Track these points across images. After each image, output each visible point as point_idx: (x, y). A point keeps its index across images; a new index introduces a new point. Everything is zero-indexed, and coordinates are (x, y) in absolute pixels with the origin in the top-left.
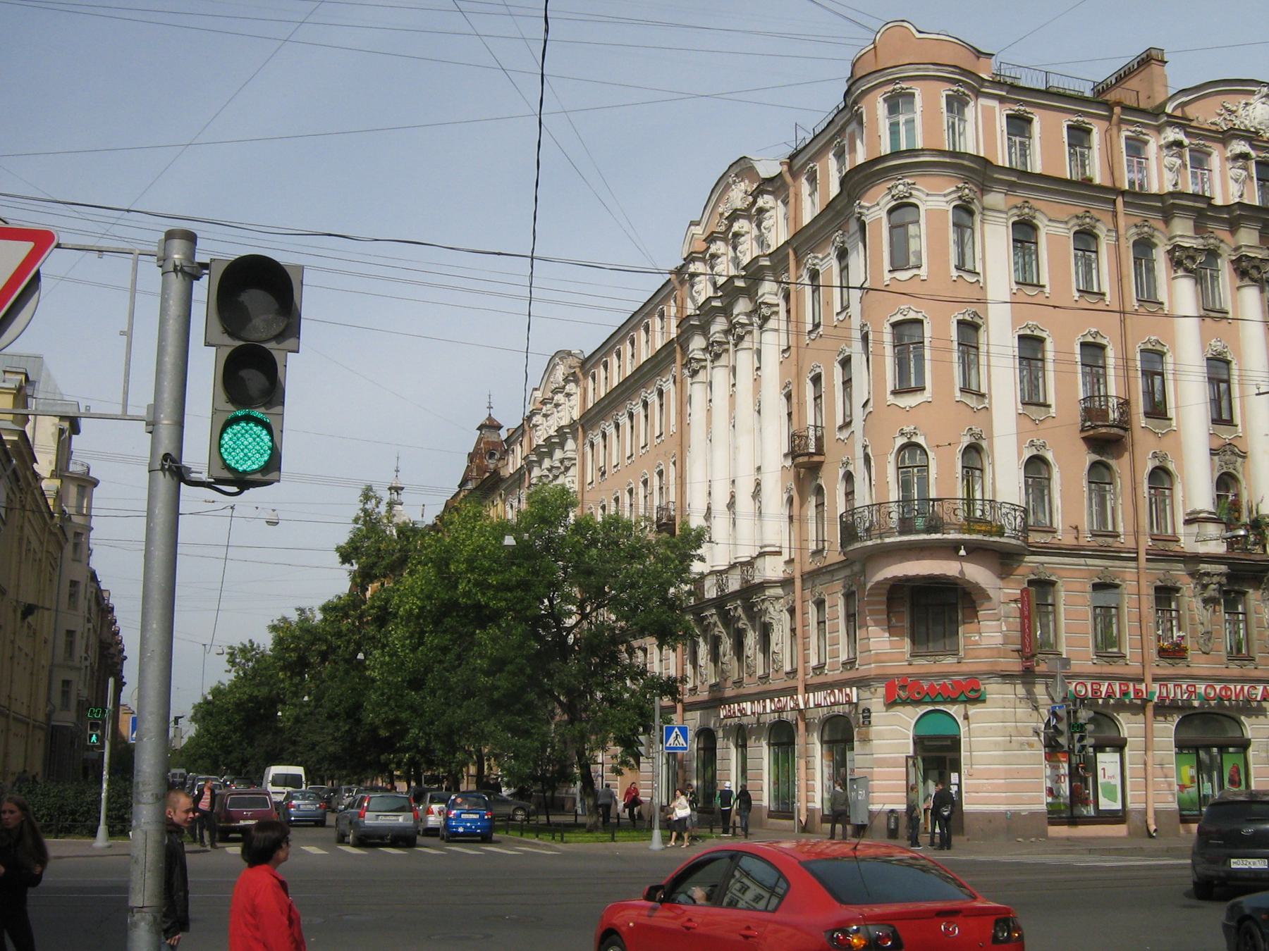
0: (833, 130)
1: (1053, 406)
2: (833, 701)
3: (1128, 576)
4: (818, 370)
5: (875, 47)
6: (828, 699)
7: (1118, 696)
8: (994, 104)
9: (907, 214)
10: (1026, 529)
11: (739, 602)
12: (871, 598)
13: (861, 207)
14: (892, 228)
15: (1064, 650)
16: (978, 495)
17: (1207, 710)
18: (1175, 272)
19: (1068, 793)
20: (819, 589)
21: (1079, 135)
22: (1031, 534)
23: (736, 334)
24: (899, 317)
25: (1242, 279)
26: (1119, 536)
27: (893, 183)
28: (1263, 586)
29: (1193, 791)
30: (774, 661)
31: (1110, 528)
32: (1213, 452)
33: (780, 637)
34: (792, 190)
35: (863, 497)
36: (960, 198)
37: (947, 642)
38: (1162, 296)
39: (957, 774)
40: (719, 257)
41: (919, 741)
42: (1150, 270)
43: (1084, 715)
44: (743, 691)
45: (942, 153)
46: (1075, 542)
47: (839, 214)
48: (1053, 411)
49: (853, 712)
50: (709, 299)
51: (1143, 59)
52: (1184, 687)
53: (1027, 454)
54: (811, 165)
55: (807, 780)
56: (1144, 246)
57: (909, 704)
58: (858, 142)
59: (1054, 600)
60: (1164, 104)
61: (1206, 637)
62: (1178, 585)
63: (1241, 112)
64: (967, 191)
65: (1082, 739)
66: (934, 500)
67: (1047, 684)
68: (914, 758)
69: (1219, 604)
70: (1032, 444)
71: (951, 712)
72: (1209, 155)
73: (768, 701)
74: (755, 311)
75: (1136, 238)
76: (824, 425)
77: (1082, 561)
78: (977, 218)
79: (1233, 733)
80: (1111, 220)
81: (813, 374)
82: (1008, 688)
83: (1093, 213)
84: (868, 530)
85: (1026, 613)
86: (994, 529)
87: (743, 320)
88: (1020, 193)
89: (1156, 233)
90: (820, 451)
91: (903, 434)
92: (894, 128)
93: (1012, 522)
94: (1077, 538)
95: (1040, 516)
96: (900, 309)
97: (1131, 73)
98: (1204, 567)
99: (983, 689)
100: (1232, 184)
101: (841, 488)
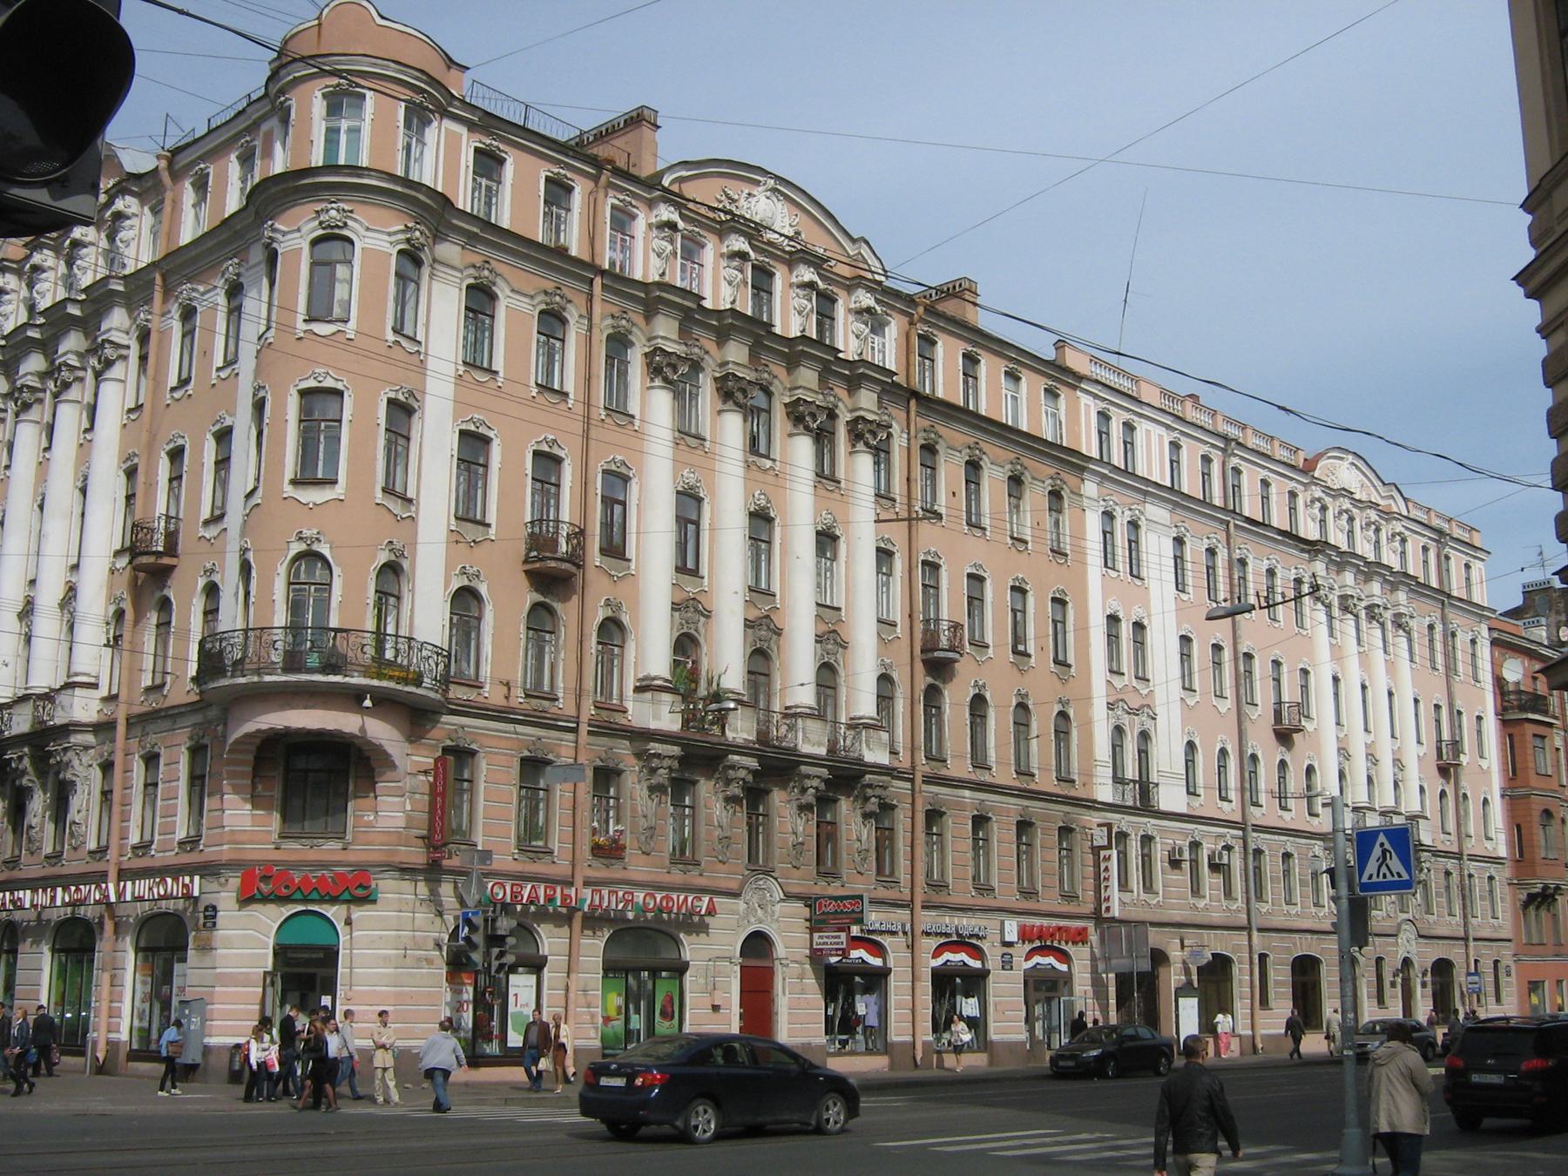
0: (242, 124)
1: (494, 526)
2: (162, 892)
3: (563, 752)
4: (180, 442)
5: (320, 25)
6: (155, 890)
7: (542, 902)
8: (462, 130)
9: (334, 250)
10: (445, 681)
11: (26, 750)
12: (234, 756)
13: (274, 230)
14: (314, 264)
15: (480, 841)
16: (390, 630)
17: (642, 925)
18: (652, 380)
19: (470, 1025)
20: (152, 738)
21: (558, 191)
22: (452, 687)
23: (58, 379)
24: (312, 383)
25: (725, 402)
26: (557, 700)
27: (323, 205)
28: (717, 775)
29: (618, 1025)
30: (72, 834)
31: (546, 688)
32: (675, 607)
33: (84, 804)
34: (169, 196)
35: (231, 617)
36: (408, 241)
37: (329, 819)
38: (634, 407)
39: (329, 997)
40: (44, 271)
41: (281, 952)
42: (623, 374)
43: (504, 925)
44: (16, 874)
45: (392, 177)
46: (503, 702)
47: (238, 235)
48: (492, 531)
49: (191, 909)
50: (19, 330)
51: (632, 118)
52: (620, 894)
53: (456, 584)
54: (202, 166)
55: (111, 1001)
56: (619, 343)
57: (272, 901)
58: (278, 146)
59: (472, 774)
60: (661, 174)
61: (648, 833)
62: (621, 766)
63: (742, 202)
64: (417, 233)
65: (501, 955)
66: (336, 630)
67: (455, 883)
68: (272, 974)
69: (667, 794)
70: (463, 572)
71: (329, 915)
72: (703, 246)
73: (59, 890)
74: (95, 349)
75: (611, 331)
76: (181, 516)
77: (510, 727)
78: (426, 271)
79: (668, 954)
80: (584, 302)
81: (171, 446)
82: (407, 886)
83: (565, 291)
84: (236, 663)
85: (440, 789)
86: (411, 676)
87: (73, 361)
88: (481, 249)
89: (634, 329)
90: (171, 548)
91: (301, 538)
92: (332, 135)
93: (432, 668)
94: (507, 698)
95: (464, 665)
96: (314, 373)
97: (614, 131)
98: (655, 747)
99: (373, 886)
100: (724, 286)
101: (198, 605)
